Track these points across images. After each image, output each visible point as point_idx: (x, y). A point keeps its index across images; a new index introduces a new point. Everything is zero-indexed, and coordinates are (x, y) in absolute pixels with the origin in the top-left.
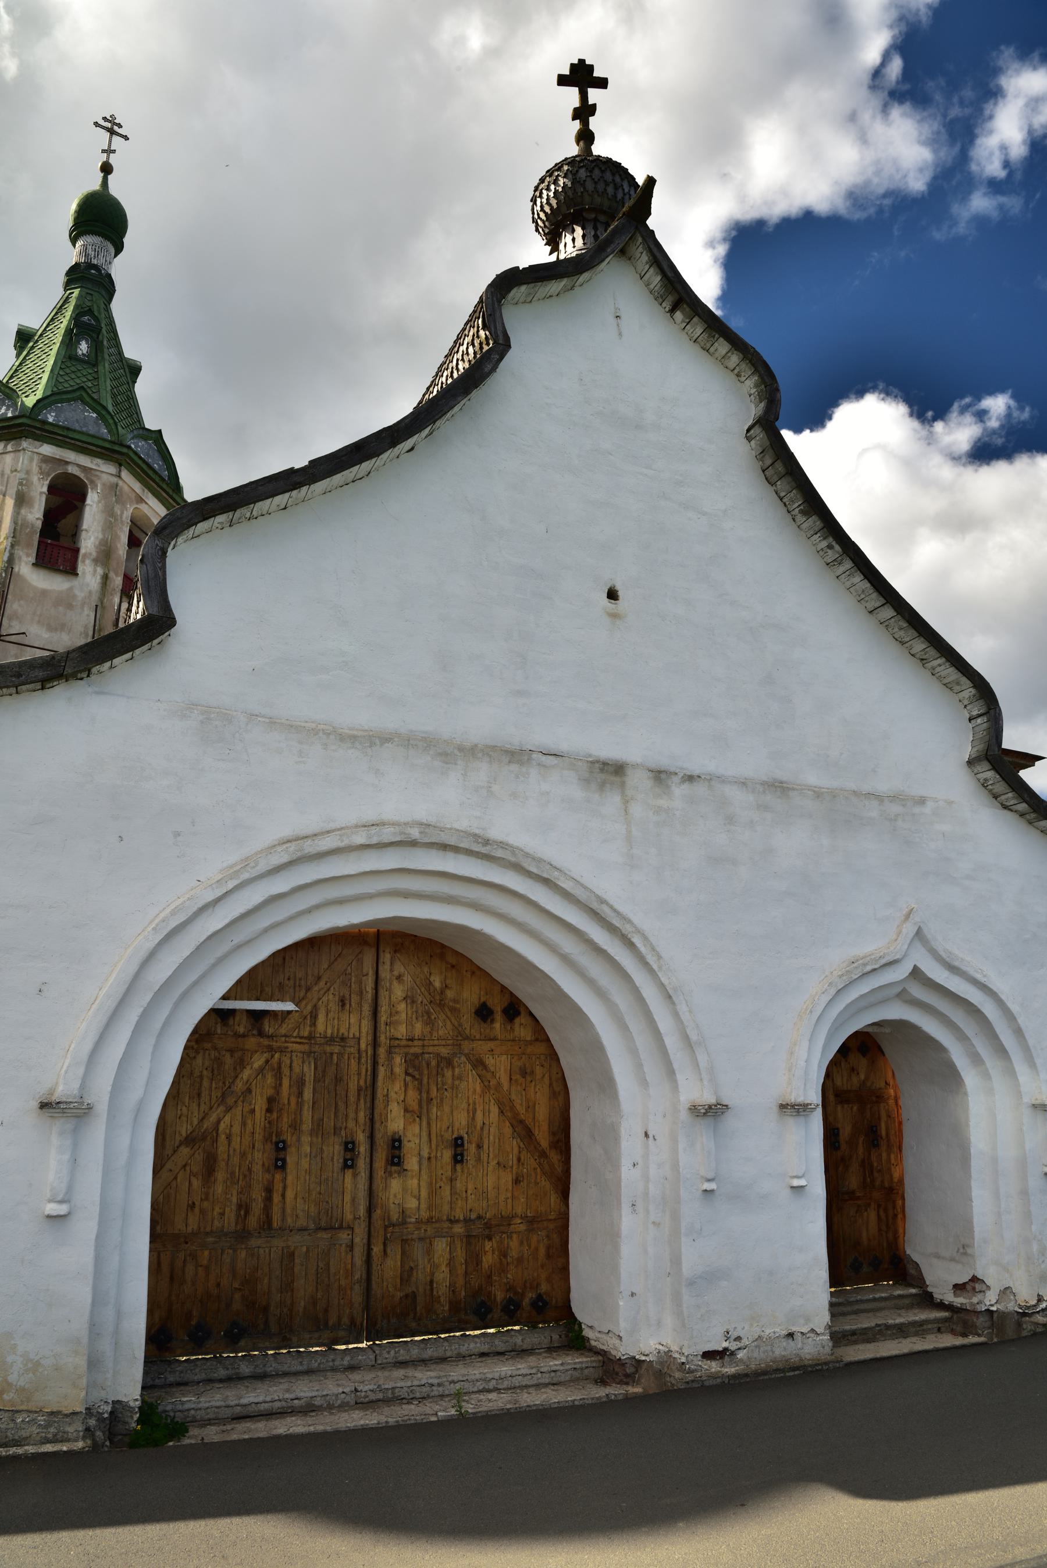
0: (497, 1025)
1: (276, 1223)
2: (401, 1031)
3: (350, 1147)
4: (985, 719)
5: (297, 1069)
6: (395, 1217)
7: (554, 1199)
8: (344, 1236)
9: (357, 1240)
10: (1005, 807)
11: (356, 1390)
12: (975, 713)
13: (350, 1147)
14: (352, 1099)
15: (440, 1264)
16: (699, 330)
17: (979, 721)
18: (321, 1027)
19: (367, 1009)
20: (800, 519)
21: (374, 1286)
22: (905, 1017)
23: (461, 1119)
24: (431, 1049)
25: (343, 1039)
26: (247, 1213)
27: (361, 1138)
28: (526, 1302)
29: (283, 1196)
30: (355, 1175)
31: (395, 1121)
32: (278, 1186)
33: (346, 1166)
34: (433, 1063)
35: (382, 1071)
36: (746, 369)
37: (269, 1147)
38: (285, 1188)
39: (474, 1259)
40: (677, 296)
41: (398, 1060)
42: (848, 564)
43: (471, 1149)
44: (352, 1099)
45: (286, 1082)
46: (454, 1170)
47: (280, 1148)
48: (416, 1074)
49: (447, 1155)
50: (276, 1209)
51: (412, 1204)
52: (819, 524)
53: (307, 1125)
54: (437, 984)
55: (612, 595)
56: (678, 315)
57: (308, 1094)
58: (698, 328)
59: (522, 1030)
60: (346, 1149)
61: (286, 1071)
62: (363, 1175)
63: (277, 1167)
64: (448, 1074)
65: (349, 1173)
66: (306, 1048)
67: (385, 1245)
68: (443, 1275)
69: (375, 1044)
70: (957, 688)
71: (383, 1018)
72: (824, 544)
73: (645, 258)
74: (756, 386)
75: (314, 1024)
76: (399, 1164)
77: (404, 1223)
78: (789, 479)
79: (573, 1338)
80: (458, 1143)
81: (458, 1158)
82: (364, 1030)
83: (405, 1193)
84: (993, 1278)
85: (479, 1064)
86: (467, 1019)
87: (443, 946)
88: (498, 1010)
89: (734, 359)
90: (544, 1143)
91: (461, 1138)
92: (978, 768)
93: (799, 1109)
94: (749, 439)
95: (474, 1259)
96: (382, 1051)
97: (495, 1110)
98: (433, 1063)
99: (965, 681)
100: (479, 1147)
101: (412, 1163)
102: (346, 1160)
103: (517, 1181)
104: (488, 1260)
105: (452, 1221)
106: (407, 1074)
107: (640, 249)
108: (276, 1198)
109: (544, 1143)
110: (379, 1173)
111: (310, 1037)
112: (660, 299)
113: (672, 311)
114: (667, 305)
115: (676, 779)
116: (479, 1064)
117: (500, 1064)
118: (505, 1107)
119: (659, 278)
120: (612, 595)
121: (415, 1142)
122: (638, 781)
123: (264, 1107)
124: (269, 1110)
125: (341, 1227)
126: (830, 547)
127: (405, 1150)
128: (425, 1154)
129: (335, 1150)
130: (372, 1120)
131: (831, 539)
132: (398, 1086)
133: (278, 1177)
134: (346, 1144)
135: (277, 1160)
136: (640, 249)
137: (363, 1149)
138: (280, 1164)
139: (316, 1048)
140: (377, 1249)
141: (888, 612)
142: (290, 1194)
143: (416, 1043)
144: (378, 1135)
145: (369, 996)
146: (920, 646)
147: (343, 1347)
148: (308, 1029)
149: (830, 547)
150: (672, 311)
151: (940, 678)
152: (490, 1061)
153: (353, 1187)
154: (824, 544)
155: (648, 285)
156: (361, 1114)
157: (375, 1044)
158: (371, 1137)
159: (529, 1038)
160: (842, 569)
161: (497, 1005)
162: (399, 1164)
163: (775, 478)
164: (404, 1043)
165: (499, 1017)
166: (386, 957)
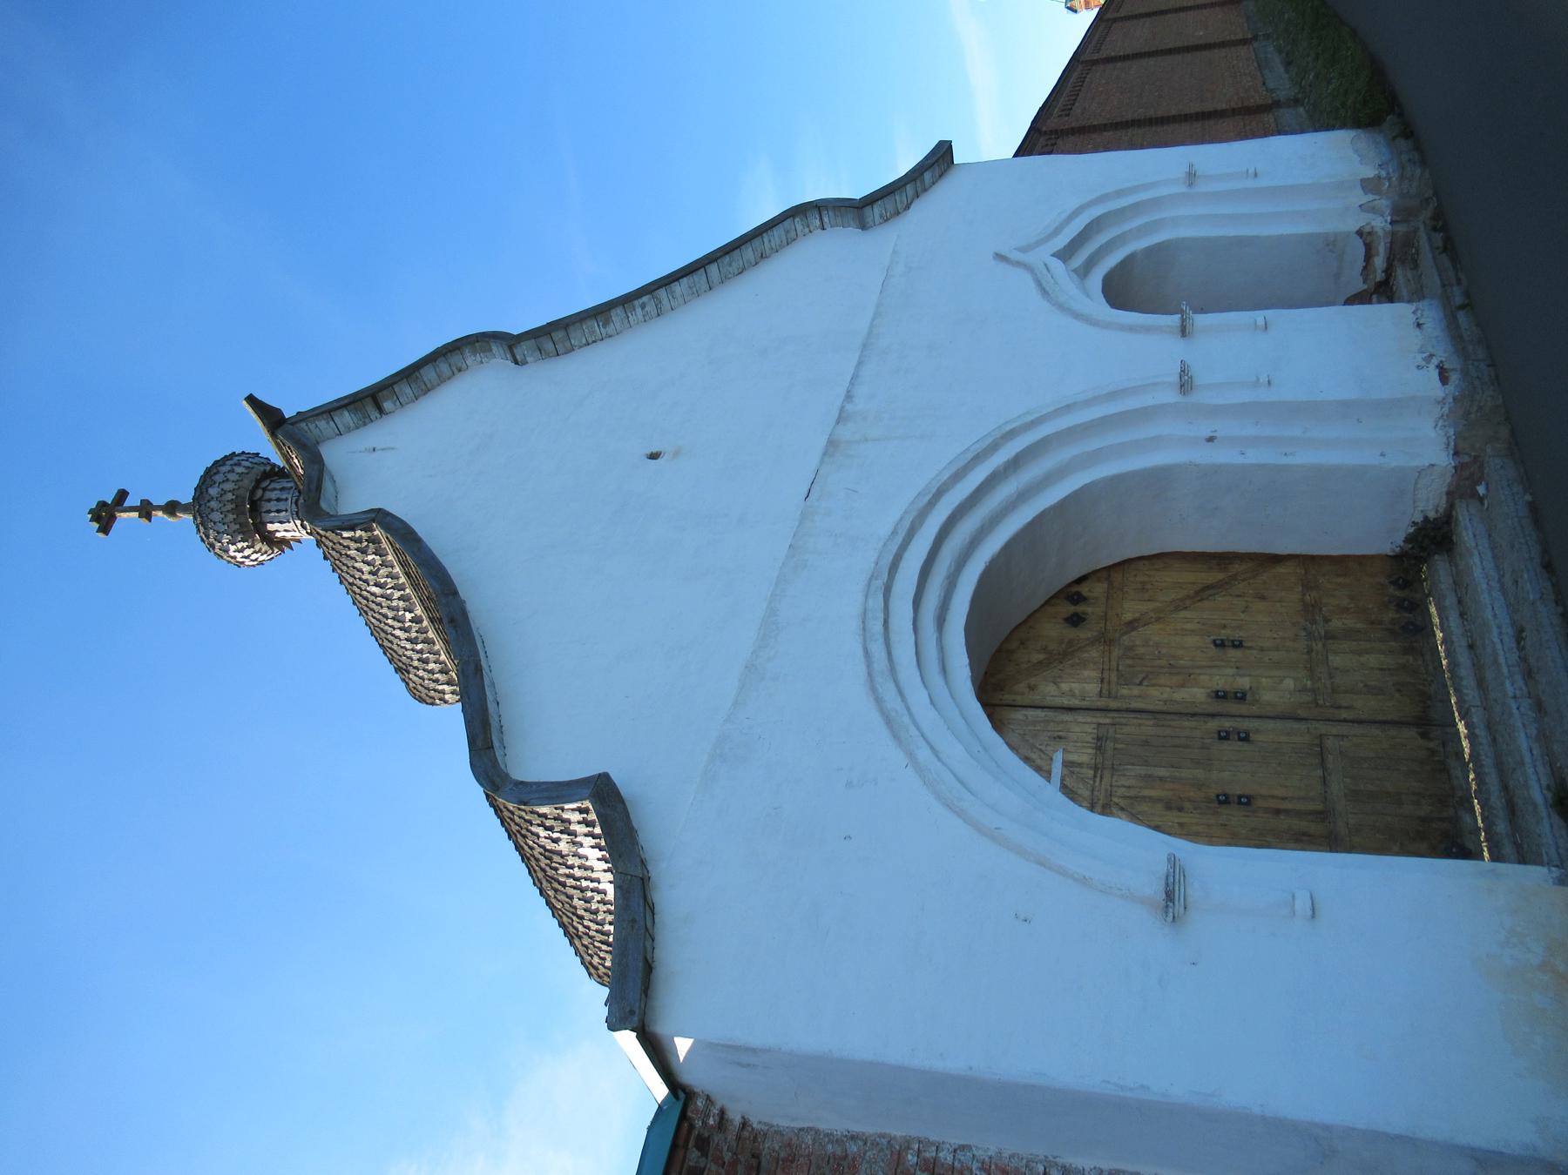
0: (1089, 610)
1: (1320, 807)
2: (1092, 688)
3: (1224, 736)
4: (824, 213)
5: (1132, 782)
6: (1307, 698)
7: (1281, 570)
8: (1330, 743)
9: (1334, 731)
10: (908, 207)
11: (1515, 697)
12: (818, 222)
13: (1224, 736)
14: (1168, 731)
15: (1362, 665)
16: (408, 390)
17: (826, 219)
18: (1084, 758)
19: (1068, 717)
20: (610, 329)
21: (1389, 717)
22: (1087, 481)
23: (1192, 641)
24: (1114, 664)
25: (1099, 739)
26: (1304, 834)
27: (1213, 725)
28: (1398, 593)
29: (1284, 799)
30: (1257, 731)
31: (1196, 694)
32: (1273, 804)
33: (1246, 739)
34: (1129, 662)
35: (1135, 705)
36: (455, 359)
37: (1224, 810)
38: (1273, 797)
39: (1349, 634)
40: (369, 400)
41: (1125, 691)
42: (662, 293)
43: (1225, 634)
44: (1168, 731)
45: (1147, 792)
46: (1250, 648)
47: (1224, 800)
48: (1141, 676)
49: (1233, 654)
50: (1301, 806)
51: (1289, 683)
52: (619, 310)
53: (1199, 773)
54: (1041, 657)
55: (654, 456)
56: (387, 405)
57: (1162, 772)
58: (405, 389)
59: (1096, 590)
60: (1227, 738)
61: (1133, 793)
62: (1255, 724)
63: (1248, 804)
64: (1142, 650)
65: (1253, 737)
66: (1107, 774)
67: (1339, 707)
68: (1372, 660)
69: (1105, 710)
70: (793, 234)
71: (1076, 702)
72: (639, 310)
73: (322, 424)
74: (474, 353)
75: (1080, 765)
76: (1244, 694)
77: (1313, 690)
78: (571, 329)
79: (1433, 538)
80: (1220, 644)
81: (1238, 645)
82: (1089, 720)
83: (1279, 688)
84: (1353, 223)
85: (1132, 625)
86: (1083, 634)
87: (999, 651)
88: (1072, 609)
89: (443, 367)
90: (1221, 576)
91: (1214, 642)
92: (870, 220)
93: (1172, 898)
94: (525, 363)
95: (1349, 634)
96: (1113, 704)
97: (1183, 614)
98: (1129, 662)
99: (786, 223)
100: (1224, 627)
101: (1244, 683)
102: (1240, 739)
103: (1263, 598)
104: (1351, 622)
105: (1310, 651)
106: (1140, 684)
107: (312, 426)
108: (1287, 805)
109: (1221, 576)
110: (1255, 709)
111: (1096, 768)
112: (366, 421)
113: (381, 411)
114: (374, 414)
115: (849, 407)
116: (1132, 625)
117: (1131, 609)
118: (1180, 605)
119: (346, 413)
120: (654, 456)
121: (1222, 679)
122: (845, 432)
123: (1176, 813)
124: (1181, 809)
125: (1321, 745)
126: (643, 306)
127: (1228, 688)
128: (1232, 671)
129: (1229, 748)
130: (1194, 715)
131: (636, 303)
132: (1154, 692)
133: (1260, 803)
134: (1221, 738)
135: (1240, 803)
136: (312, 426)
137: (1227, 724)
138: (1246, 801)
139: (1108, 763)
140: (1344, 715)
141: (713, 269)
142: (1280, 792)
143: (1106, 675)
144: (1211, 709)
145: (1051, 714)
146: (748, 253)
147: (1465, 743)
148: (1084, 770)
149: (643, 306)
150: (381, 411)
151: (782, 247)
152: (1128, 616)
153: (1268, 733)
154: (639, 310)
155: (349, 430)
156: (1186, 724)
157: (1105, 710)
158: (1213, 716)
159: (1105, 585)
160: (665, 301)
161: (1068, 609)
162: (1244, 694)
163: (567, 344)
164: (1105, 686)
165: (1080, 608)
166: (1008, 698)
